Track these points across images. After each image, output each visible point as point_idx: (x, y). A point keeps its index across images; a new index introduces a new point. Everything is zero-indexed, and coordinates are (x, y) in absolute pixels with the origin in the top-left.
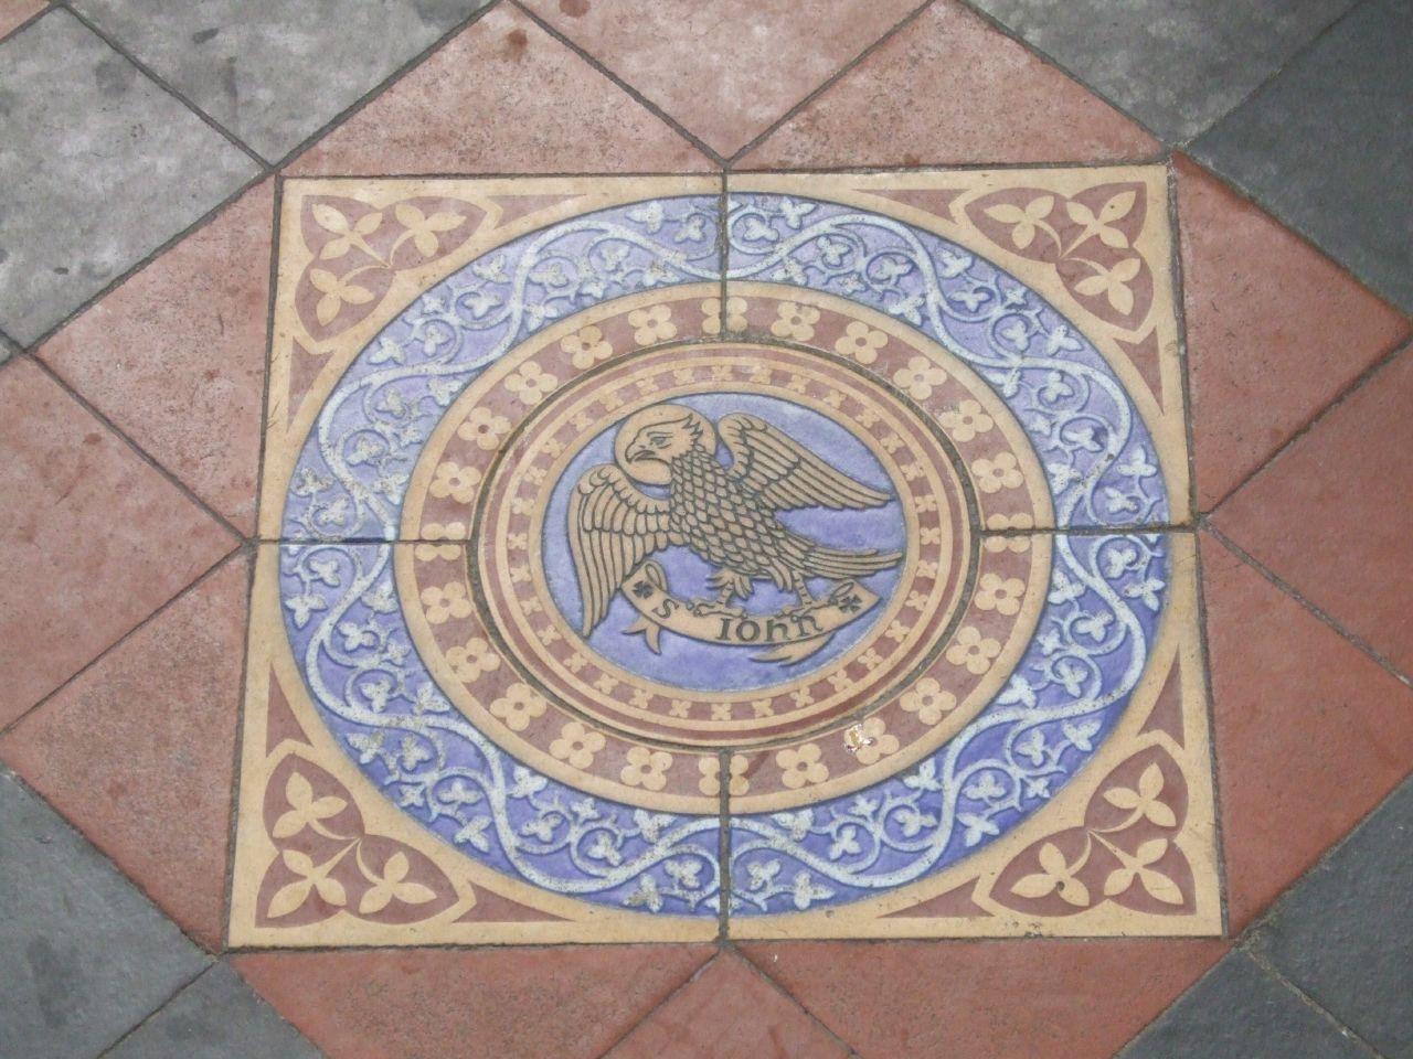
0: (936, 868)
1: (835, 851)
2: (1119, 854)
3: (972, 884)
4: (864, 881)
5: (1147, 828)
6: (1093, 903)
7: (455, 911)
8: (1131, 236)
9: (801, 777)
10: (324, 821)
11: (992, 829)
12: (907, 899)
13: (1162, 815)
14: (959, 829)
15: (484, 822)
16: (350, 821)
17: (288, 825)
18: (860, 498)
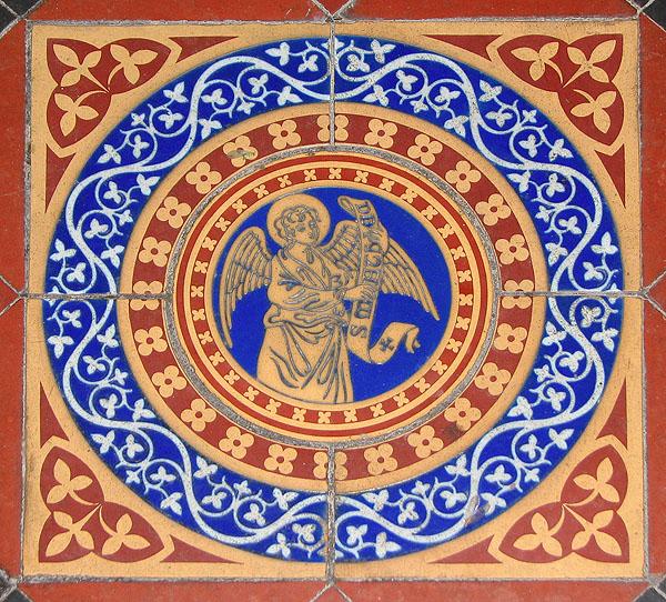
0: (469, 528)
1: (264, 78)
2: (91, 78)
3: (489, 541)
4: (243, 59)
5: (73, 92)
6: (109, 46)
7: (498, 43)
8: (612, 74)
9: (286, 127)
10: (77, 492)
11: (167, 93)
12: (443, 552)
13: (611, 495)
14: (188, 93)
15: (483, 98)
16: (94, 493)
17: (608, 99)
18: (396, 272)
